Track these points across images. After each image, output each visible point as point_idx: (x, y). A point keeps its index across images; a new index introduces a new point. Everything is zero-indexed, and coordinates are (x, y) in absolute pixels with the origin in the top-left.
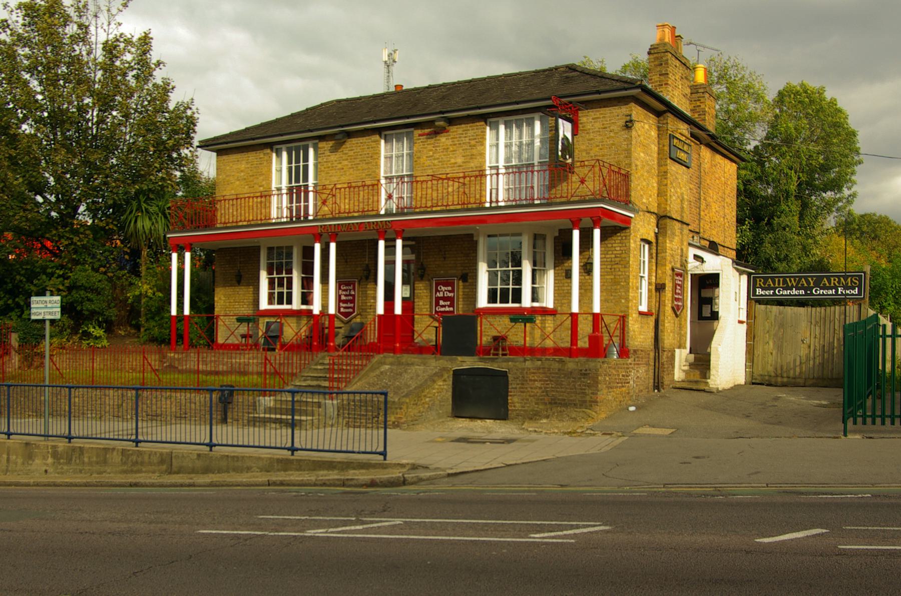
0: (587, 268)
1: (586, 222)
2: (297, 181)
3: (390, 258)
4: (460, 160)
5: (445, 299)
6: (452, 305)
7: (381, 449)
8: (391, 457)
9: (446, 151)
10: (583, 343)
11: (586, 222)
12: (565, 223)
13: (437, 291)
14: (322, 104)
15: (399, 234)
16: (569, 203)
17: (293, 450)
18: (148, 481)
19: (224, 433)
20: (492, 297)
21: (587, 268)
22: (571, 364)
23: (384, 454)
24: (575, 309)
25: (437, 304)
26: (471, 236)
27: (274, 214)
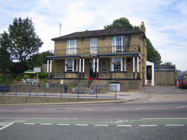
0: (82, 64)
1: (136, 56)
2: (119, 44)
3: (96, 62)
4: (107, 44)
5: (104, 70)
6: (106, 71)
7: (115, 96)
8: (117, 98)
9: (105, 43)
10: (136, 77)
11: (136, 56)
12: (132, 56)
13: (102, 68)
14: (96, 31)
15: (98, 57)
16: (133, 52)
17: (97, 97)
18: (80, 103)
19: (98, 95)
20: (115, 68)
21: (82, 64)
22: (134, 81)
23: (116, 97)
24: (138, 71)
25: (102, 70)
26: (109, 58)
27: (113, 51)
